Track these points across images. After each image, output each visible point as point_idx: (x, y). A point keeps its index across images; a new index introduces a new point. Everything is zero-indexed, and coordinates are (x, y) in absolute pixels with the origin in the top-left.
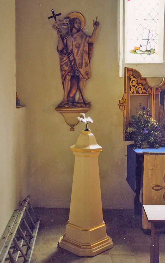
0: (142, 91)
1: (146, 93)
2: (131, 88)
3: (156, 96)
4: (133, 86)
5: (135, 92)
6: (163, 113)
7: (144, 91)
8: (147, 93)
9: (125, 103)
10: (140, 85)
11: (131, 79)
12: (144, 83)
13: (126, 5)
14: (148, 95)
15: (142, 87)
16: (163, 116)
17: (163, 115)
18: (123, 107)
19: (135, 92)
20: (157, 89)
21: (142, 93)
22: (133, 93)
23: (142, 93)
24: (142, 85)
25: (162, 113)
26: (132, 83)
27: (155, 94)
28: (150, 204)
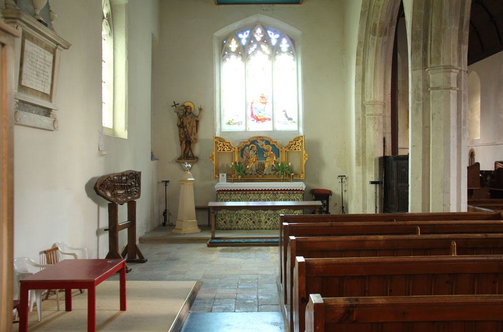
7: (229, 149)
10: (226, 146)
20: (238, 148)
22: (220, 151)
24: (227, 146)
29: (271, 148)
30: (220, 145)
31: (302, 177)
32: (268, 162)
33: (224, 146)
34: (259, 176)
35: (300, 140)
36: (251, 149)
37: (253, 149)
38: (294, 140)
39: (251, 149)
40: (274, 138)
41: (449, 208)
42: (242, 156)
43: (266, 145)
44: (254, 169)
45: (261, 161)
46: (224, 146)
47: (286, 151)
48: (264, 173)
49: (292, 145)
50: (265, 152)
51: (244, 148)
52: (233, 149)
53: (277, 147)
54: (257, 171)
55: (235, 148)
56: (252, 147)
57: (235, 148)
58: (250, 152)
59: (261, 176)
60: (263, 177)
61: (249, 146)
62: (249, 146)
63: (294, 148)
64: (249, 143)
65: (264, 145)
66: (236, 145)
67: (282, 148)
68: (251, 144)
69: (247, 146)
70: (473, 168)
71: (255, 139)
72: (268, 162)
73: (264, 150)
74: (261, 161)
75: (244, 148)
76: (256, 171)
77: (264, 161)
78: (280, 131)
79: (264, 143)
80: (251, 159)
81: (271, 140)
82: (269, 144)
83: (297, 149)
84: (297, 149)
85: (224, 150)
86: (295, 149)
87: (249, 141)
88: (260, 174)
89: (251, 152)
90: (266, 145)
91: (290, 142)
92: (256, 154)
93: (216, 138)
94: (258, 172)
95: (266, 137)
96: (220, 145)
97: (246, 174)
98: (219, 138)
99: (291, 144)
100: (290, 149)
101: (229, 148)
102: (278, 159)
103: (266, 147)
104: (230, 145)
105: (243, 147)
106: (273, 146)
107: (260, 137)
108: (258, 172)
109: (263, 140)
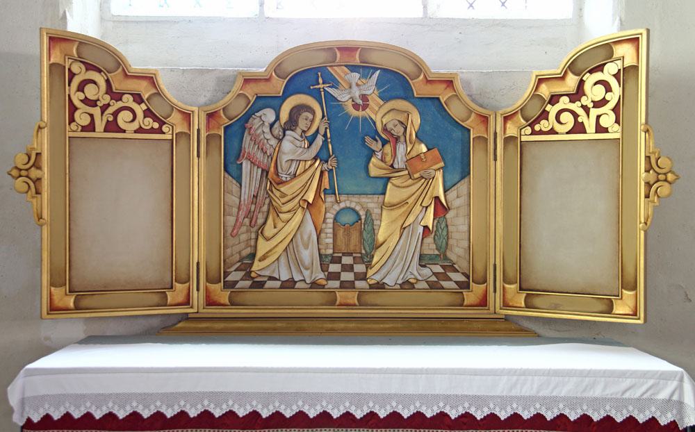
0: (137, 121)
1: (160, 131)
2: (73, 109)
3: (207, 142)
4: (86, 101)
5: (100, 125)
6: (239, 209)
7: (149, 123)
8: (165, 128)
9: (39, 168)
10: (128, 100)
11: (72, 75)
12: (146, 91)
13: (524, 155)
14: (172, 140)
15: (139, 109)
16: (237, 220)
17: (237, 217)
18: (28, 184)
19: (100, 125)
20: (211, 116)
21: (136, 132)
22: (91, 127)
23: (140, 130)
24: (138, 99)
25: (235, 210)
26: (606, 130)
27: (203, 135)
28: (515, 20)
29: (416, 119)
30: (90, 91)
31: (619, 308)
32: (392, 206)
33: (118, 97)
34: (341, 296)
35: (611, 68)
36: (292, 123)
37: (302, 124)
38: (572, 67)
39: (292, 123)
40: (437, 60)
41: (66, 28)
42: (232, 167)
43: (385, 98)
44: (308, 254)
45: (352, 202)
46: (118, 97)
47: (509, 140)
48: (374, 277)
49: (554, 99)
50: (376, 146)
51: (248, 116)
52: (175, 118)
53: (456, 111)
54: (324, 260)
55: (187, 116)
56: (297, 111)
57: (187, 116)
58: (287, 145)
59: (352, 297)
60: (362, 304)
61: (275, 102)
62: (275, 102)
63: (567, 118)
64: (278, 86)
65: (375, 100)
66: (197, 99)
67: (485, 119)
68: (287, 93)
69: (263, 101)
70: (81, 101)
71: (317, 60)
72: (392, 206)
73: (375, 136)
74: (352, 202)
75: (248, 116)
76: (324, 268)
77: (371, 203)
78: (202, 343)
79: (370, 87)
80: (296, 185)
81: (419, 67)
82: (407, 94)
83: (590, 125)
84: (590, 125)
85: (112, 126)
86: (579, 128)
87: (278, 67)
88: (346, 285)
89: (291, 146)
90: (385, 98)
91: (541, 81)
92: (321, 156)
93: (57, 40)
94: (334, 268)
95: (384, 48)
96: (90, 91)
97: (259, 285)
98: (83, 42)
99: (545, 91)
100: (544, 125)
101: (148, 113)
102: (462, 187)
103: (381, 114)
104: (159, 94)
105: (239, 109)
106: (432, 107)
107: (348, 49)
108: (334, 268)
109: (365, 69)
